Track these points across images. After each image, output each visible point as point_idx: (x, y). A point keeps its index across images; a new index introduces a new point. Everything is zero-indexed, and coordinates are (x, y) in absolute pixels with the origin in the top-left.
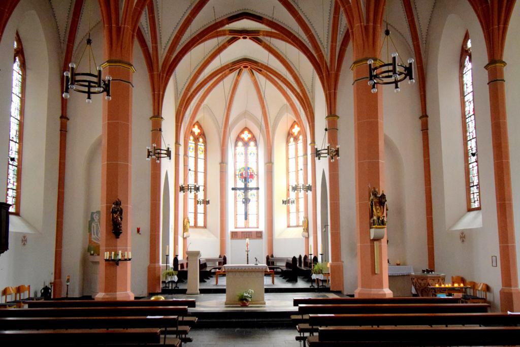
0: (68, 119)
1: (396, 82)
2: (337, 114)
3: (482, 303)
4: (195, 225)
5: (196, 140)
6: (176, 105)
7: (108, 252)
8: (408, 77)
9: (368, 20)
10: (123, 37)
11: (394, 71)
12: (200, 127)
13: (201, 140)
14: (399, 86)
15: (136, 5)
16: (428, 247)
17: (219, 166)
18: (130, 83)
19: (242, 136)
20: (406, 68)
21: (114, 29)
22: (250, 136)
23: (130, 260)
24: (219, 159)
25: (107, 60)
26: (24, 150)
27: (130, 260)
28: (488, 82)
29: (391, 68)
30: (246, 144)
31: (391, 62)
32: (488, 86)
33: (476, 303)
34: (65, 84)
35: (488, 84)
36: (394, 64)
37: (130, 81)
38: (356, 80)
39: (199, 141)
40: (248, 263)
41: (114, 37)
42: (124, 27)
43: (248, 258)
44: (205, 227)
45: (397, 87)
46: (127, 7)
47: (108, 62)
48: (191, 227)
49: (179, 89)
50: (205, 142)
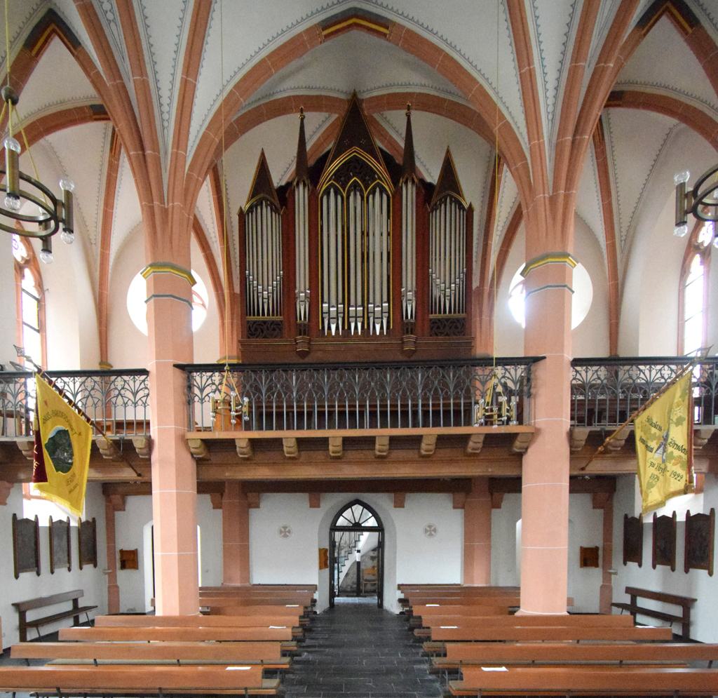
4: (636, 597)
7: (287, 666)
9: (555, 188)
10: (172, 223)
15: (189, 170)
16: (114, 543)
18: (565, 286)
21: (157, 211)
23: (95, 660)
25: (150, 262)
27: (95, 660)
28: (146, 299)
32: (145, 305)
33: (647, 665)
35: (146, 302)
37: (566, 284)
38: (154, 296)
40: (710, 667)
41: (158, 222)
42: (173, 207)
43: (495, 641)
47: (151, 266)
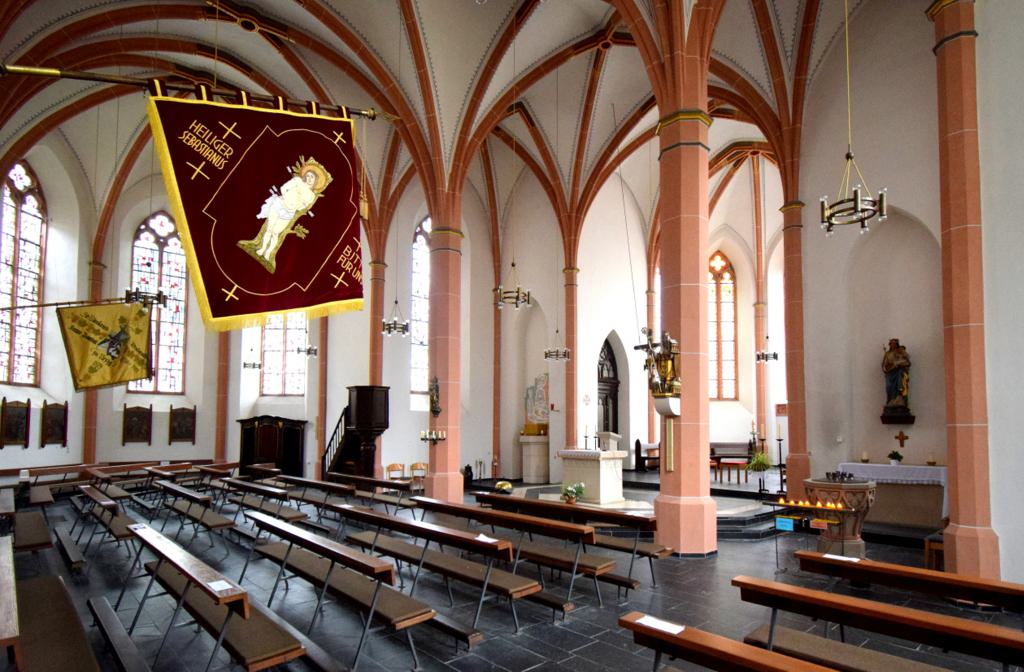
0: (977, 35)
1: (862, 221)
2: (103, 262)
3: (175, 96)
5: (718, 276)
6: (644, 233)
8: (878, 213)
11: (855, 208)
12: (724, 258)
13: (727, 275)
14: (866, 224)
17: (752, 310)
19: (153, 223)
20: (874, 203)
22: (723, 263)
24: (752, 299)
26: (337, 421)
29: (851, 204)
30: (19, 197)
31: (852, 197)
34: (498, 298)
36: (855, 199)
39: (722, 278)
44: (736, 399)
45: (863, 226)
46: (648, 52)
48: (712, 399)
49: (647, 220)
50: (734, 277)
